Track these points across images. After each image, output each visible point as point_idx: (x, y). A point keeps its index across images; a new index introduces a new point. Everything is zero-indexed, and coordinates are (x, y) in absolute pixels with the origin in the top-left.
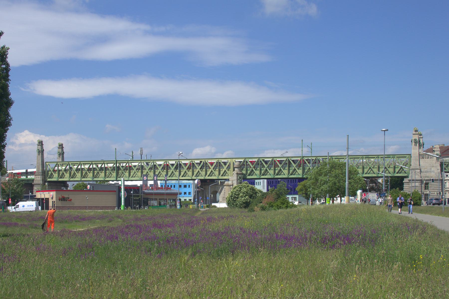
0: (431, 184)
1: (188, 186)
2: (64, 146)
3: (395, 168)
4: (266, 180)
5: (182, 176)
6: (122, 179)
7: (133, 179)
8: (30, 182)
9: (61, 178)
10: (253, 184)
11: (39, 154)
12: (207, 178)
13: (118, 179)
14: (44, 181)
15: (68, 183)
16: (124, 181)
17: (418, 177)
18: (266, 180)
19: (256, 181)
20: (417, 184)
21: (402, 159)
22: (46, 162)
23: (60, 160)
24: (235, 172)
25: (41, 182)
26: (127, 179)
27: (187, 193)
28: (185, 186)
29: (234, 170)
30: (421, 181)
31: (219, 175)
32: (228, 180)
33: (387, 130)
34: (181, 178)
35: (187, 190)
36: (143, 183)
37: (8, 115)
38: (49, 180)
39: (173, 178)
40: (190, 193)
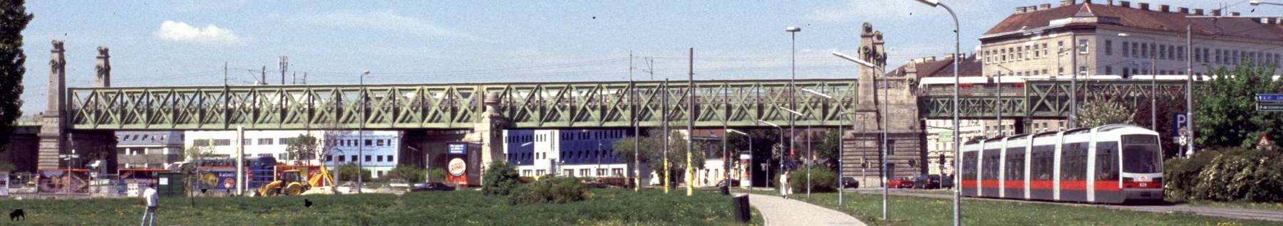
0: (898, 143)
1: (385, 143)
2: (110, 53)
3: (729, 108)
4: (557, 132)
5: (373, 122)
6: (239, 127)
7: (264, 126)
8: (32, 132)
9: (101, 123)
10: (531, 138)
11: (54, 71)
12: (426, 125)
13: (231, 126)
14: (66, 129)
15: (117, 134)
16: (244, 130)
17: (871, 126)
18: (557, 132)
19: (537, 132)
20: (869, 144)
21: (841, 88)
22: (70, 90)
23: (102, 84)
24: (487, 114)
25: (57, 132)
26: (250, 126)
27: (385, 158)
28: (380, 142)
29: (484, 109)
30: (879, 137)
31: (824, 117)
32: (472, 130)
33: (798, 30)
34: (369, 125)
35: (384, 151)
36: (448, 149)
37: (20, 38)
38: (77, 127)
39: (352, 126)
40: (390, 158)
